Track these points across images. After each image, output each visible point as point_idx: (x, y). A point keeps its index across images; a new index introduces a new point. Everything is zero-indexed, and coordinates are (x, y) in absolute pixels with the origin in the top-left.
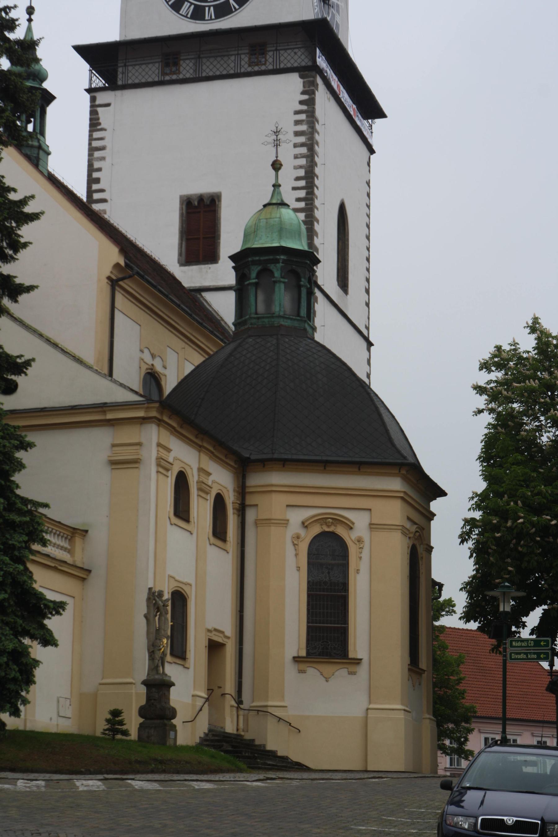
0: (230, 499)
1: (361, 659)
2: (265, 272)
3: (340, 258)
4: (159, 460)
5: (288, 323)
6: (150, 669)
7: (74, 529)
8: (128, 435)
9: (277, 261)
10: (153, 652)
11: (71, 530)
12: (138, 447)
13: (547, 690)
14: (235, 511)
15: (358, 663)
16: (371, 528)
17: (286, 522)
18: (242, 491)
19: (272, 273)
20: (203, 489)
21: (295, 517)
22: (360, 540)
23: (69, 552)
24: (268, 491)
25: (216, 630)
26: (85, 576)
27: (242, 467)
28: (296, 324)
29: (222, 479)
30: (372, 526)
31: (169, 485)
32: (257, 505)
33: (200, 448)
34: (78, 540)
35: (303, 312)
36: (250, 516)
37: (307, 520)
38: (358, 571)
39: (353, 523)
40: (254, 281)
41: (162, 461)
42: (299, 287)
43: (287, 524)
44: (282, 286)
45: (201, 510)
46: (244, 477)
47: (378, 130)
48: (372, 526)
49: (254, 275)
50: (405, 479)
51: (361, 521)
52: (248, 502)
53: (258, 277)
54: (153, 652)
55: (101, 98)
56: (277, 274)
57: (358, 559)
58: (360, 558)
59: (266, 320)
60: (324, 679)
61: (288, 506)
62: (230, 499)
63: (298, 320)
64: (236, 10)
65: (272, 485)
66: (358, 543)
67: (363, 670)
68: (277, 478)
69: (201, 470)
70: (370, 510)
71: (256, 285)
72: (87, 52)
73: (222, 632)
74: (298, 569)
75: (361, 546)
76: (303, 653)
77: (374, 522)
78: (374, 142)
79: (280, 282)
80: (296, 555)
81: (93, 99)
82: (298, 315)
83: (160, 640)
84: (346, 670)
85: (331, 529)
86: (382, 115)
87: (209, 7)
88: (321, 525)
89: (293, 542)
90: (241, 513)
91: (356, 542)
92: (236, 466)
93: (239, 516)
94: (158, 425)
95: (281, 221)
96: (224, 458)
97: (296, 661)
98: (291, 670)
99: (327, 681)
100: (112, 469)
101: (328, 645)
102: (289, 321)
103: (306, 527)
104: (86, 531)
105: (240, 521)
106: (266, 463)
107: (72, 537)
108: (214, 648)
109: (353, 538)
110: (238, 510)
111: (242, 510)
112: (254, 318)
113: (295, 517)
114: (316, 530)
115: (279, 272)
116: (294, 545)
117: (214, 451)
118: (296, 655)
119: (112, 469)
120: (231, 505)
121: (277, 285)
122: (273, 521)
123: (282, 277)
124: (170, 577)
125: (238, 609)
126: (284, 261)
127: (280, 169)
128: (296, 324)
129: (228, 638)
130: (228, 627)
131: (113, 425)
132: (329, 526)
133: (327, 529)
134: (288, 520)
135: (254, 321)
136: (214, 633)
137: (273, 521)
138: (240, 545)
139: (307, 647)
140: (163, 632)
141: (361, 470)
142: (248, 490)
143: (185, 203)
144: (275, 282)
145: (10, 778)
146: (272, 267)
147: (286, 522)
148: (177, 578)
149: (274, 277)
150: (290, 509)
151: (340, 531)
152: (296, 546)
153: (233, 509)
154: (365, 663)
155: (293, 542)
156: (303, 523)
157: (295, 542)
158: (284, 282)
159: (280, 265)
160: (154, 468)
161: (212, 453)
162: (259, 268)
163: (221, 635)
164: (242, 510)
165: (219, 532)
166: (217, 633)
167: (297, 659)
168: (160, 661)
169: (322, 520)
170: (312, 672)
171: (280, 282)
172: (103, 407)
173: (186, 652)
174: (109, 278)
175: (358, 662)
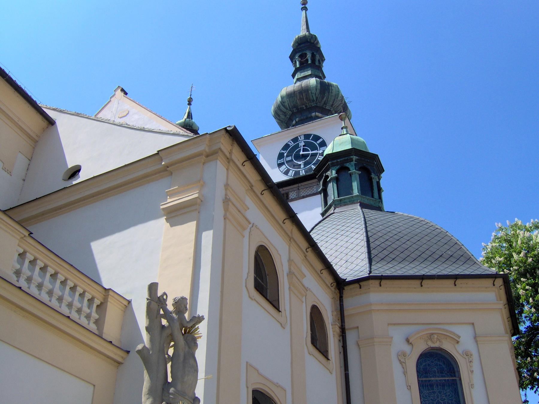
9: (351, 160)
13: (158, 283)
19: (348, 169)
31: (305, 313)
36: (351, 337)
38: (472, 386)
39: (459, 337)
51: (465, 334)
57: (470, 372)
58: (472, 372)
61: (389, 324)
66: (466, 357)
69: (290, 261)
74: (409, 388)
75: (471, 359)
109: (460, 352)
115: (354, 167)
120: (331, 327)
138: (343, 368)
145: (247, 271)
146: (347, 165)
151: (447, 346)
152: (403, 364)
155: (400, 361)
157: (402, 360)
159: (353, 163)
162: (338, 167)
165: (318, 340)
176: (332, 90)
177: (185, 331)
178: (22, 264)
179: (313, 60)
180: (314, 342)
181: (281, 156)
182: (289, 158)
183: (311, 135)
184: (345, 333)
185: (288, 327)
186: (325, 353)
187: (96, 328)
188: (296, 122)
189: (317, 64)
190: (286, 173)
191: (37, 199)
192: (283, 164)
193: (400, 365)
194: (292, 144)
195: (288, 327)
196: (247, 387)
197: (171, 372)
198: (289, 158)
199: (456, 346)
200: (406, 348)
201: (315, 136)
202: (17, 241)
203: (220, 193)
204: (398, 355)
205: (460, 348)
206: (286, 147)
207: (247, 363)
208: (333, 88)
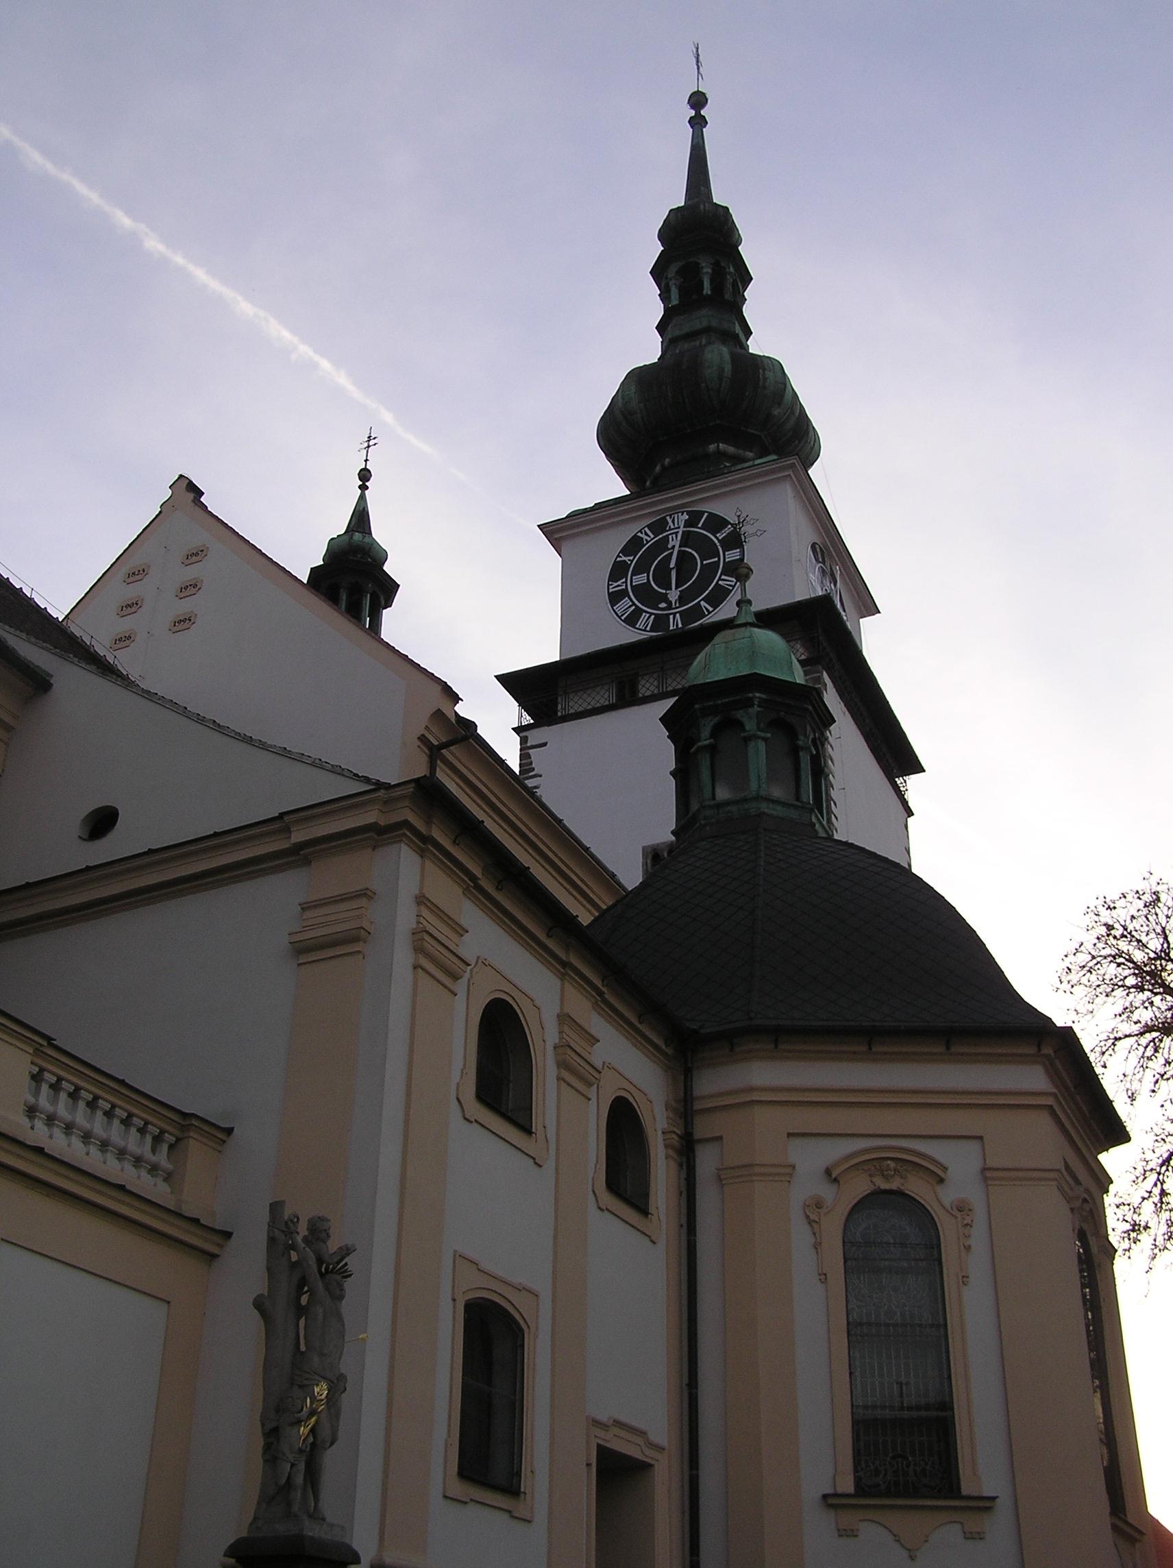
0: (657, 1122)
1: (994, 1498)
2: (729, 725)
3: (869, 601)
4: (418, 936)
5: (779, 811)
6: (266, 1499)
7: (185, 1115)
8: (333, 875)
9: (748, 703)
10: (275, 1430)
11: (175, 1117)
12: (363, 902)
14: (671, 1152)
15: (988, 1509)
16: (985, 1179)
17: (788, 1170)
18: (686, 1109)
19: (740, 725)
20: (579, 1072)
21: (811, 1159)
22: (962, 1208)
23: (165, 1180)
24: (745, 1101)
25: (617, 1423)
26: (215, 1250)
27: (688, 1050)
28: (794, 814)
29: (629, 1064)
30: (987, 1173)
32: (720, 1138)
33: (563, 968)
34: (195, 1148)
35: (808, 796)
36: (707, 1161)
37: (837, 1164)
39: (945, 1169)
40: (707, 742)
41: (427, 938)
42: (795, 751)
43: (791, 1175)
44: (762, 746)
45: (571, 1121)
46: (688, 1073)
47: (913, 785)
48: (988, 1174)
49: (706, 732)
50: (1052, 1073)
51: (961, 1163)
52: (698, 1135)
53: (713, 735)
54: (275, 1430)
55: (535, 737)
56: (750, 726)
58: (968, 1248)
59: (733, 808)
60: (905, 1554)
61: (789, 1135)
62: (657, 1122)
63: (796, 807)
64: (709, 612)
65: (752, 1089)
66: (959, 1214)
67: (999, 1526)
68: (765, 1073)
69: (565, 1019)
70: (981, 1138)
71: (713, 750)
72: (515, 683)
73: (642, 1433)
74: (823, 1277)
75: (968, 1221)
76: (847, 1485)
77: (990, 1163)
78: (911, 797)
79: (759, 737)
80: (817, 1246)
81: (523, 741)
82: (798, 798)
83: (306, 1388)
84: (958, 1526)
85: (894, 1185)
86: (919, 769)
87: (674, 614)
88: (871, 1176)
89: (808, 1217)
90: (684, 1159)
91: (955, 1212)
92: (669, 1051)
93: (681, 1165)
94: (422, 853)
95: (753, 643)
96: (634, 1020)
97: (831, 1506)
98: (818, 1528)
99: (912, 1558)
100: (299, 965)
101: (908, 1466)
102: (779, 808)
103: (836, 1180)
104: (229, 1131)
105: (684, 1175)
106: (733, 1040)
107: (178, 1140)
108: (616, 1472)
109: (947, 1204)
110: (680, 1152)
111: (686, 1150)
112: (710, 807)
113: (811, 1159)
114: (860, 1187)
116: (810, 1222)
117: (604, 989)
118: (830, 1491)
119: (299, 965)
121: (752, 744)
122: (757, 1170)
123: (759, 729)
124: (459, 1257)
125: (686, 1380)
126: (762, 703)
127: (747, 577)
128: (794, 814)
129: (661, 1449)
130: (650, 1415)
131: (307, 862)
132: (887, 1178)
133: (885, 1186)
134: (794, 1167)
135: (708, 813)
136: (616, 1431)
137: (757, 1170)
139: (856, 1471)
140: (316, 1359)
141: (953, 1050)
142: (697, 1106)
143: (650, 856)
144: (747, 740)
145: (461, 1066)
146: (739, 715)
147: (788, 1170)
148: (485, 1265)
149: (744, 730)
150: (797, 1142)
151: (916, 1187)
152: (815, 1225)
153: (666, 1146)
154: (1004, 1505)
155: (808, 1217)
156: (828, 1172)
157: (812, 1217)
158: (765, 739)
160: (403, 957)
161: (601, 994)
162: (716, 719)
163: (639, 1440)
164: (686, 1150)
165: (624, 1177)
166: (624, 1434)
167: (831, 1501)
168: (302, 1466)
169: (875, 1164)
170: (872, 1533)
171: (757, 737)
172: (282, 822)
173: (519, 1474)
174: (422, 739)
175: (985, 1504)
176: (765, 379)
177: (327, 1269)
178: (37, 1093)
179: (718, 287)
180: (615, 1184)
181: (618, 571)
182: (641, 579)
183: (704, 512)
184: (694, 1152)
185: (550, 1165)
186: (640, 1204)
187: (169, 1190)
188: (664, 468)
189: (728, 296)
190: (631, 620)
191: (28, 886)
192: (622, 594)
193: (807, 1227)
194: (649, 538)
195: (550, 1165)
196: (454, 1300)
197: (305, 1337)
198: (641, 579)
199: (938, 1188)
200: (827, 1192)
201: (712, 516)
202: (29, 1058)
203: (406, 917)
204: (806, 1206)
205: (948, 1194)
206: (633, 545)
207: (455, 1252)
208: (768, 374)
